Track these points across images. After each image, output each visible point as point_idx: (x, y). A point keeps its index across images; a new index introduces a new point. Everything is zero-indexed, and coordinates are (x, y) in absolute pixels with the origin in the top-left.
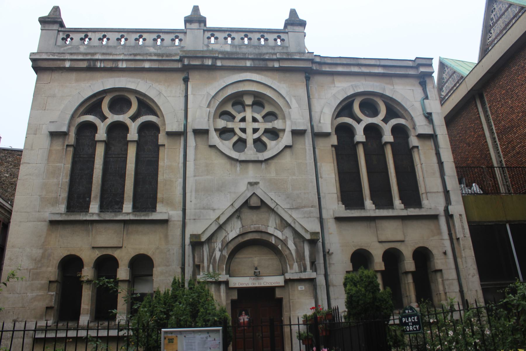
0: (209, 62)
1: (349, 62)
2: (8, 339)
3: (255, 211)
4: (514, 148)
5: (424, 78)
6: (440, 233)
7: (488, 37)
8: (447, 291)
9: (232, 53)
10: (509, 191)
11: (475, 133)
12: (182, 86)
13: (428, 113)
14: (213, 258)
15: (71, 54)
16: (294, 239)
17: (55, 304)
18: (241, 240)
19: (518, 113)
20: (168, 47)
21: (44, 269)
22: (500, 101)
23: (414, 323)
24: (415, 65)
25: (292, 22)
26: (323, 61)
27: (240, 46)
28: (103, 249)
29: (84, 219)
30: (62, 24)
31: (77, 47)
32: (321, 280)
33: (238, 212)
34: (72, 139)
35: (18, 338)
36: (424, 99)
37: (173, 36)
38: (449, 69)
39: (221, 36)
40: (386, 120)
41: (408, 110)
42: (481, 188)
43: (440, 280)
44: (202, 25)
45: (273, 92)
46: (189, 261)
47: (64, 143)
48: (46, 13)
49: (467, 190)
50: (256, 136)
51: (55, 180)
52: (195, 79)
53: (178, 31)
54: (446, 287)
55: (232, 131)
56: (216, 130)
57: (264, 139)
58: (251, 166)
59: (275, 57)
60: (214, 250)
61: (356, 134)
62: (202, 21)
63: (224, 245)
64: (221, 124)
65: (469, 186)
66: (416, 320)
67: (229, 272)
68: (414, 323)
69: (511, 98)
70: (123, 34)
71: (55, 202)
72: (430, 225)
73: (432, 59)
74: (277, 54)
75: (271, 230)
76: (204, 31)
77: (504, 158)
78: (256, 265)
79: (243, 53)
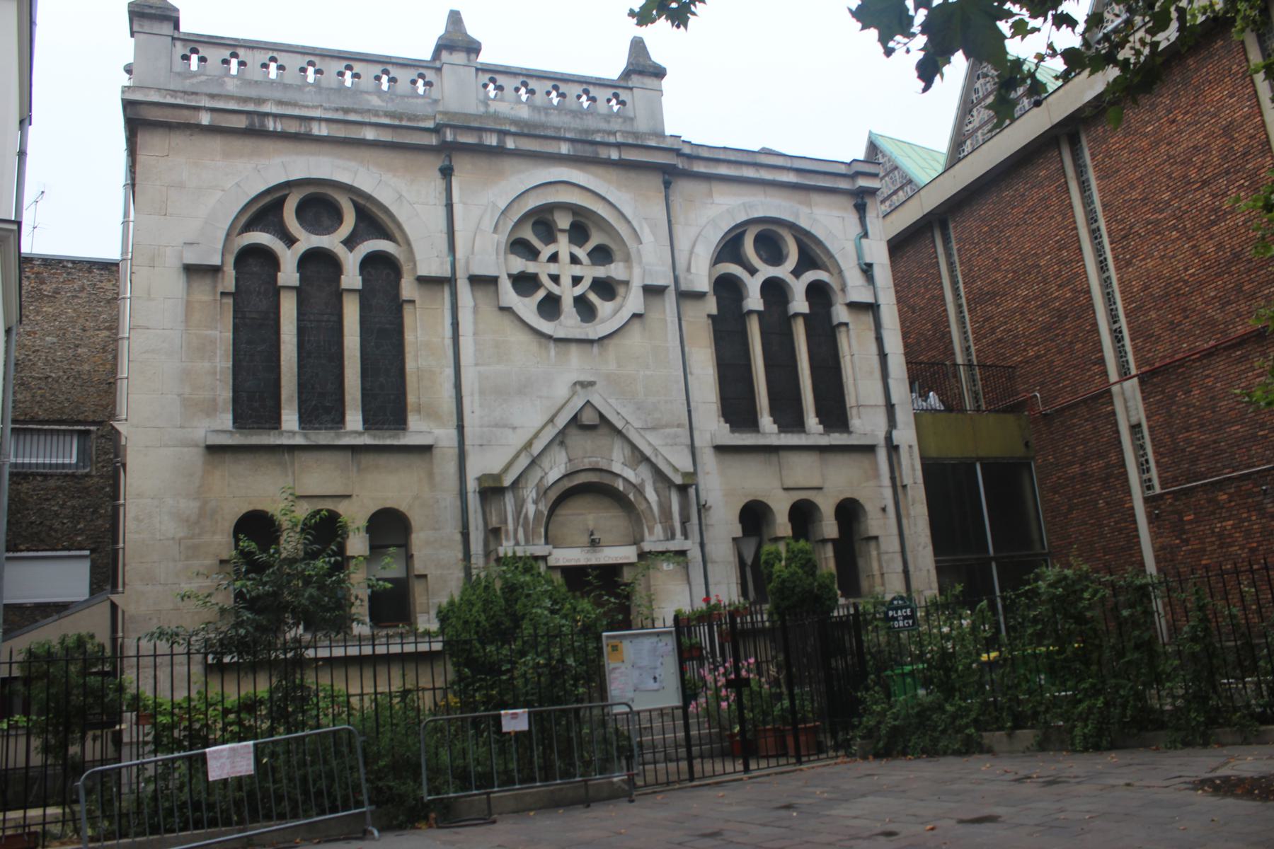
0: (492, 140)
1: (740, 159)
2: (132, 667)
3: (588, 432)
4: (993, 330)
5: (862, 198)
6: (877, 475)
8: (885, 570)
10: (979, 406)
11: (927, 290)
12: (439, 183)
14: (522, 516)
16: (654, 483)
18: (568, 484)
19: (1007, 271)
20: (408, 97)
22: (977, 244)
23: (906, 618)
24: (851, 172)
25: (640, 69)
26: (695, 152)
29: (278, 442)
32: (695, 553)
34: (229, 280)
35: (147, 667)
36: (861, 238)
38: (886, 159)
39: (508, 83)
40: (797, 273)
41: (837, 256)
42: (941, 401)
43: (874, 553)
44: (171, 26)
45: (608, 208)
46: (476, 519)
47: (215, 287)
49: (921, 404)
50: (578, 290)
51: (207, 365)
52: (465, 172)
54: (884, 565)
57: (593, 297)
58: (574, 349)
59: (612, 139)
60: (524, 501)
61: (747, 297)
62: (473, 48)
64: (519, 264)
65: (924, 397)
66: (909, 613)
67: (547, 543)
68: (906, 618)
71: (211, 409)
72: (862, 461)
74: (618, 135)
75: (617, 468)
77: (975, 344)
78: (591, 528)
79: (554, 127)
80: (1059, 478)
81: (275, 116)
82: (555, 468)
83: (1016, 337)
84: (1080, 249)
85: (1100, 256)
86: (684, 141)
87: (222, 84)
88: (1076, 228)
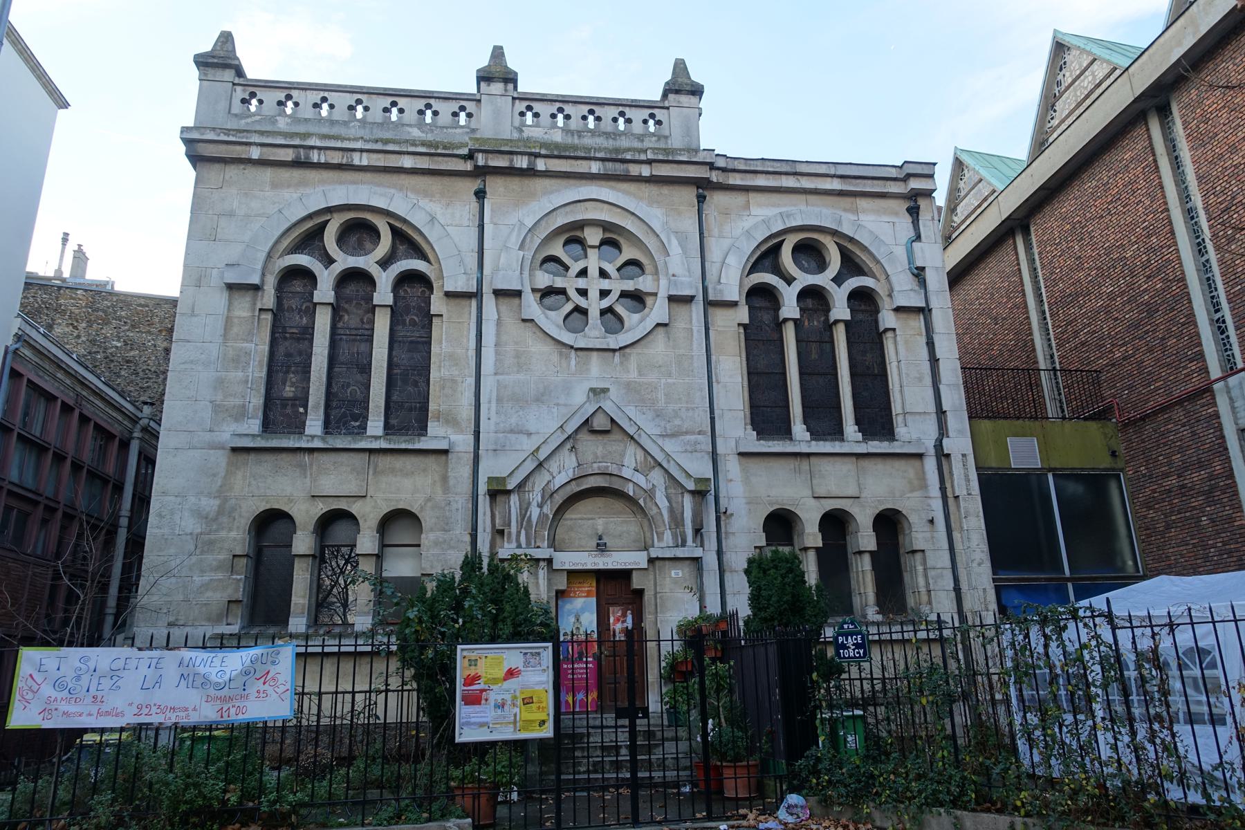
0: (522, 162)
5: (916, 201)
6: (924, 486)
7: (1049, 118)
8: (931, 587)
9: (566, 147)
11: (1009, 299)
12: (474, 205)
13: (917, 268)
15: (262, 133)
17: (243, 595)
18: (574, 488)
20: (447, 128)
21: (223, 534)
27: (579, 133)
28: (330, 500)
29: (297, 445)
30: (239, 72)
31: (272, 120)
33: (571, 440)
34: (268, 298)
37: (454, 106)
39: (545, 110)
43: (920, 568)
44: (511, 86)
46: (484, 522)
48: (207, 46)
50: (605, 303)
51: (240, 374)
53: (466, 97)
55: (562, 292)
56: (534, 290)
57: (619, 309)
59: (643, 157)
62: (510, 79)
63: (547, 496)
67: (553, 544)
69: (1079, 241)
70: (359, 96)
71: (241, 414)
72: (909, 468)
73: (935, 164)
75: (626, 473)
76: (514, 99)
77: (1058, 350)
80: (1154, 491)
81: (320, 148)
82: (562, 471)
83: (1101, 339)
84: (1172, 232)
85: (1198, 237)
86: (717, 155)
87: (274, 122)
88: (1167, 210)
